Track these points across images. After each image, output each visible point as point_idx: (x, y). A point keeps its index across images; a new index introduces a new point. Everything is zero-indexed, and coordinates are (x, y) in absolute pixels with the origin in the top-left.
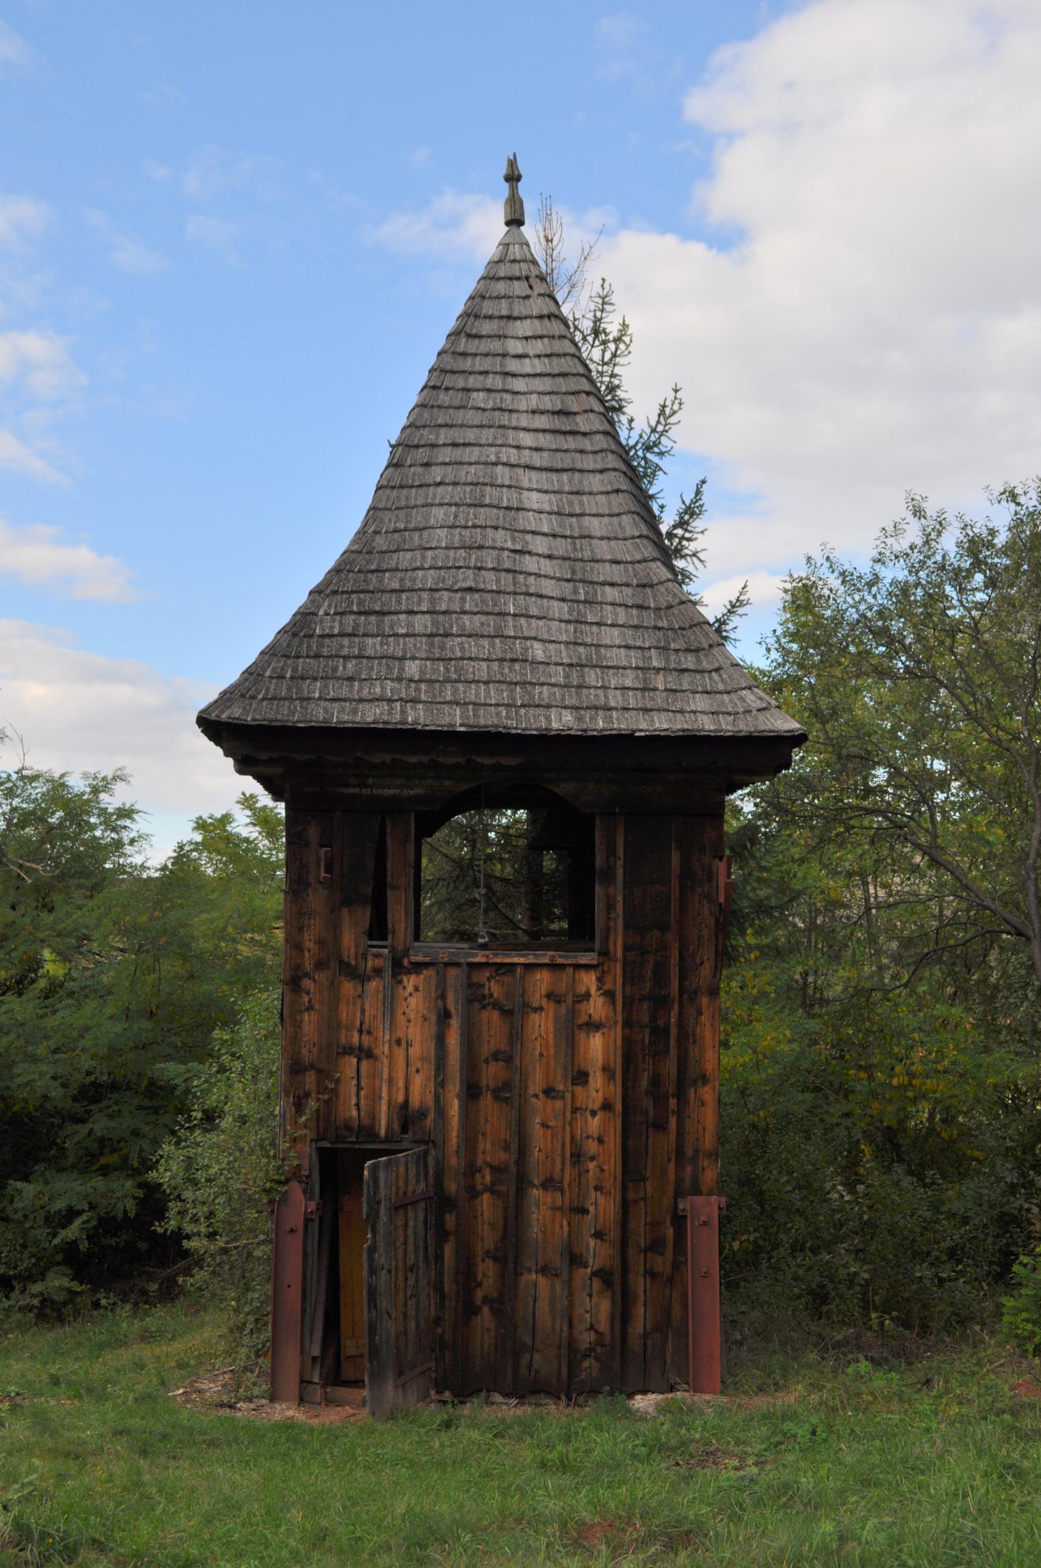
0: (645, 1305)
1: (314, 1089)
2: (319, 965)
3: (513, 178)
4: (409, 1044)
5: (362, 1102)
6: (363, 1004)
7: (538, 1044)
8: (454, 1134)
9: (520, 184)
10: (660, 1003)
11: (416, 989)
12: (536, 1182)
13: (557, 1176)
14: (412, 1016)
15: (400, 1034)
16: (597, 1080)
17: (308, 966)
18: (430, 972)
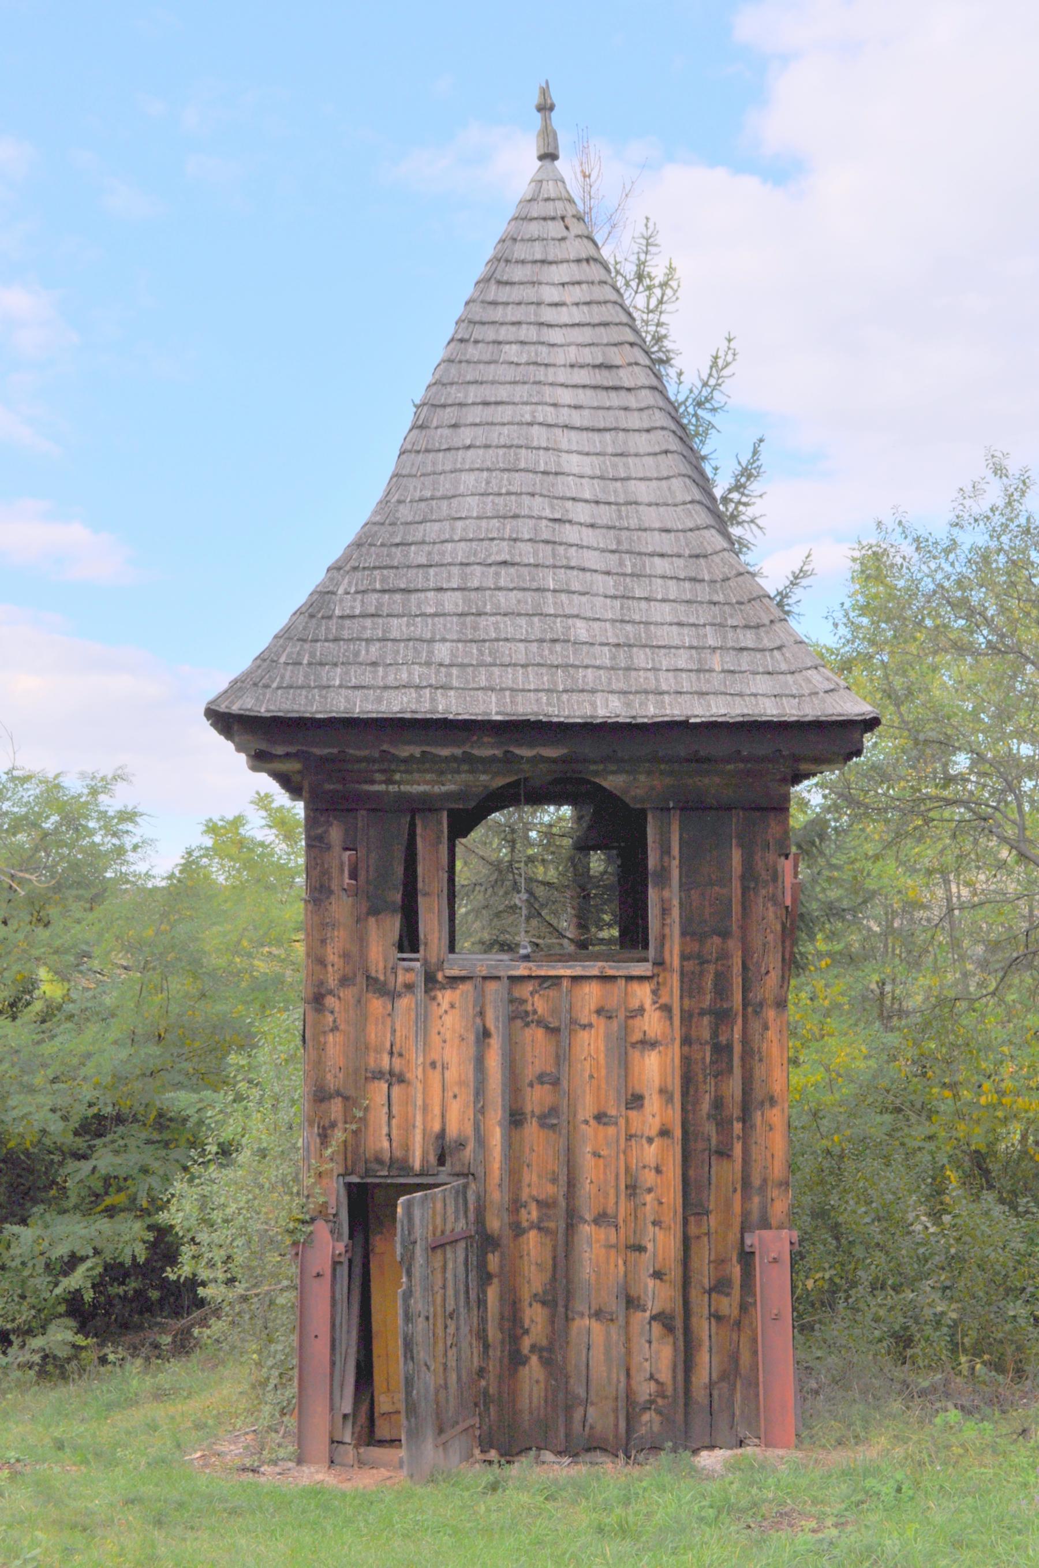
0: (710, 1351)
2: (345, 981)
3: (545, 108)
6: (393, 1023)
7: (587, 1065)
8: (496, 1165)
9: (553, 114)
10: (721, 1016)
11: (452, 1006)
12: (588, 1217)
13: (610, 1210)
17: (332, 982)
18: (466, 987)
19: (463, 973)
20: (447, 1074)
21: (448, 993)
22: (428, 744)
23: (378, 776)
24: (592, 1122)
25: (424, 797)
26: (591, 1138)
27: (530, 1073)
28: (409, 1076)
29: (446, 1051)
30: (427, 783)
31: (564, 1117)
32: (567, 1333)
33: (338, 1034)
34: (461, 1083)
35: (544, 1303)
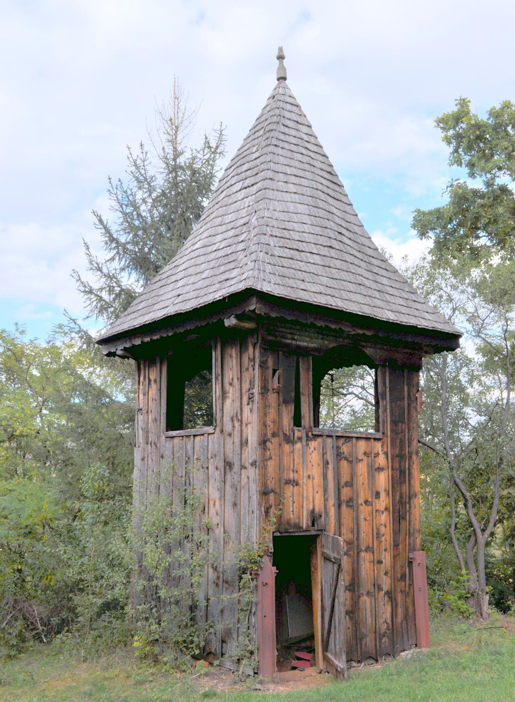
1: (273, 503)
2: (274, 435)
4: (313, 479)
5: (295, 510)
7: (361, 478)
9: (284, 61)
11: (315, 449)
12: (363, 549)
13: (371, 545)
14: (314, 463)
15: (309, 473)
16: (383, 495)
17: (269, 436)
18: (319, 440)
19: (320, 433)
20: (314, 481)
21: (313, 442)
22: (331, 322)
23: (289, 336)
24: (364, 504)
25: (306, 349)
26: (364, 511)
27: (343, 481)
28: (300, 482)
29: (314, 470)
30: (307, 342)
31: (355, 502)
32: (358, 602)
33: (272, 461)
34: (319, 486)
35: (350, 590)
